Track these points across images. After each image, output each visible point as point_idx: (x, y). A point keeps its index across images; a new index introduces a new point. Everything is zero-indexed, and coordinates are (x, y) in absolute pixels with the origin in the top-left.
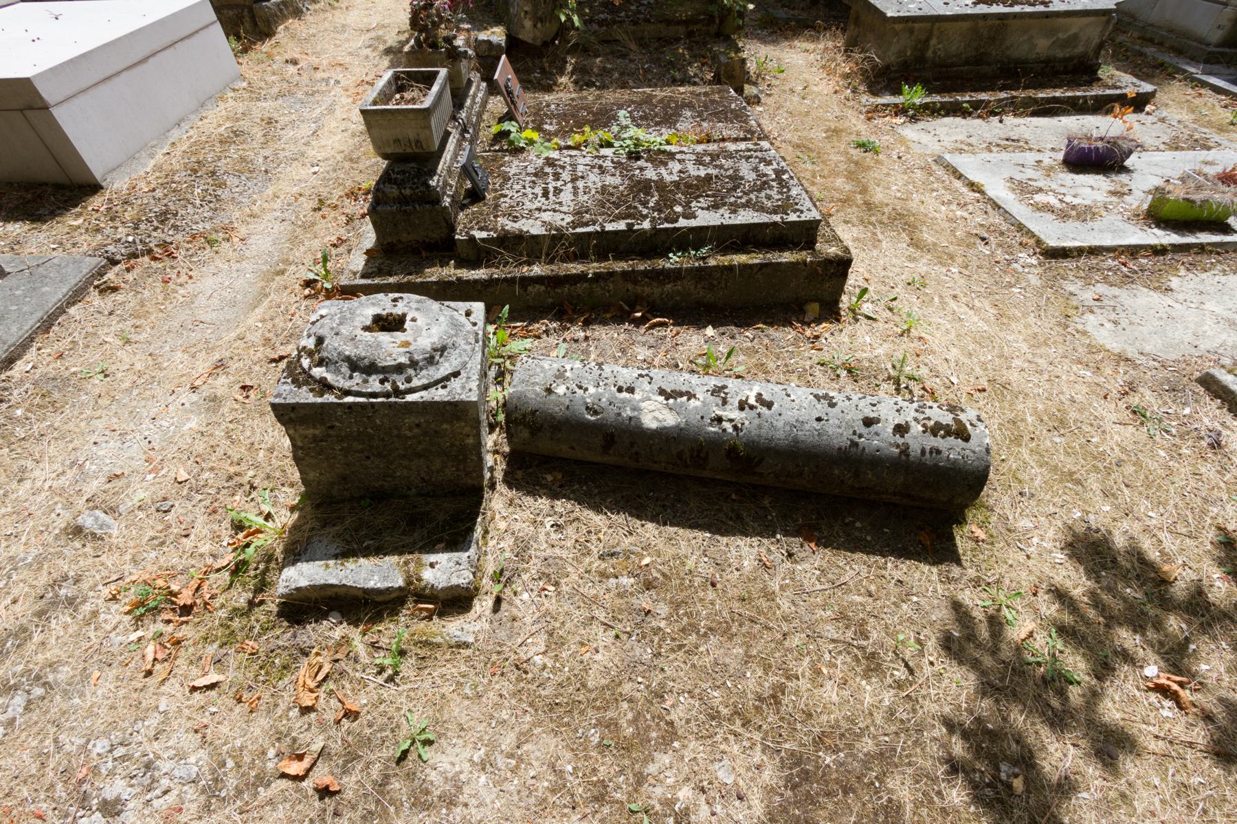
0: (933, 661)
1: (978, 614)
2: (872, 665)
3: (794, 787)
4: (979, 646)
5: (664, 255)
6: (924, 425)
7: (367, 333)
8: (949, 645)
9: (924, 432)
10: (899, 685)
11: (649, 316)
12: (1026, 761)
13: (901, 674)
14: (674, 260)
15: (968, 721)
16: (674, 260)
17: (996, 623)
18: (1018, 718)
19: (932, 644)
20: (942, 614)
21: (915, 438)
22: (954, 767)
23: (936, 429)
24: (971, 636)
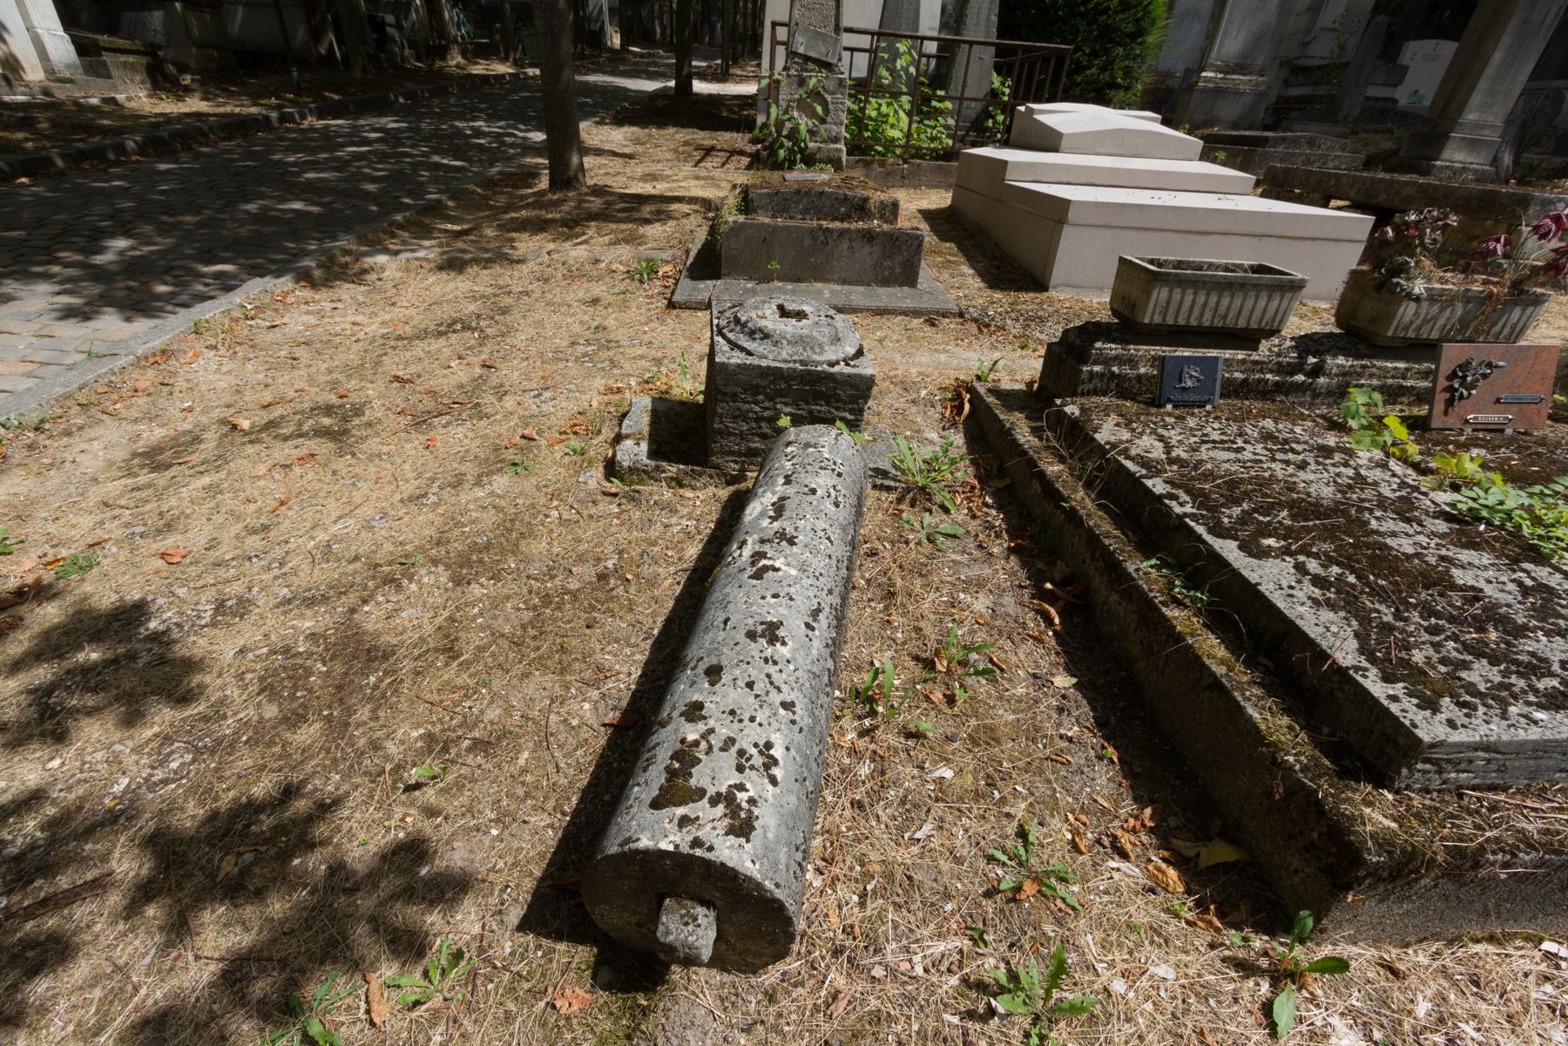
0: (404, 821)
1: (433, 919)
2: (436, 744)
3: (369, 651)
4: (393, 897)
5: (1146, 548)
6: (696, 743)
7: (829, 356)
8: (413, 851)
9: (683, 741)
10: (399, 768)
11: (1061, 604)
12: (236, 890)
13: (414, 774)
14: (1143, 569)
15: (321, 830)
16: (1143, 569)
17: (409, 946)
18: (277, 907)
19: (427, 827)
20: (456, 857)
21: (676, 731)
22: (289, 792)
23: (686, 757)
24: (409, 893)
